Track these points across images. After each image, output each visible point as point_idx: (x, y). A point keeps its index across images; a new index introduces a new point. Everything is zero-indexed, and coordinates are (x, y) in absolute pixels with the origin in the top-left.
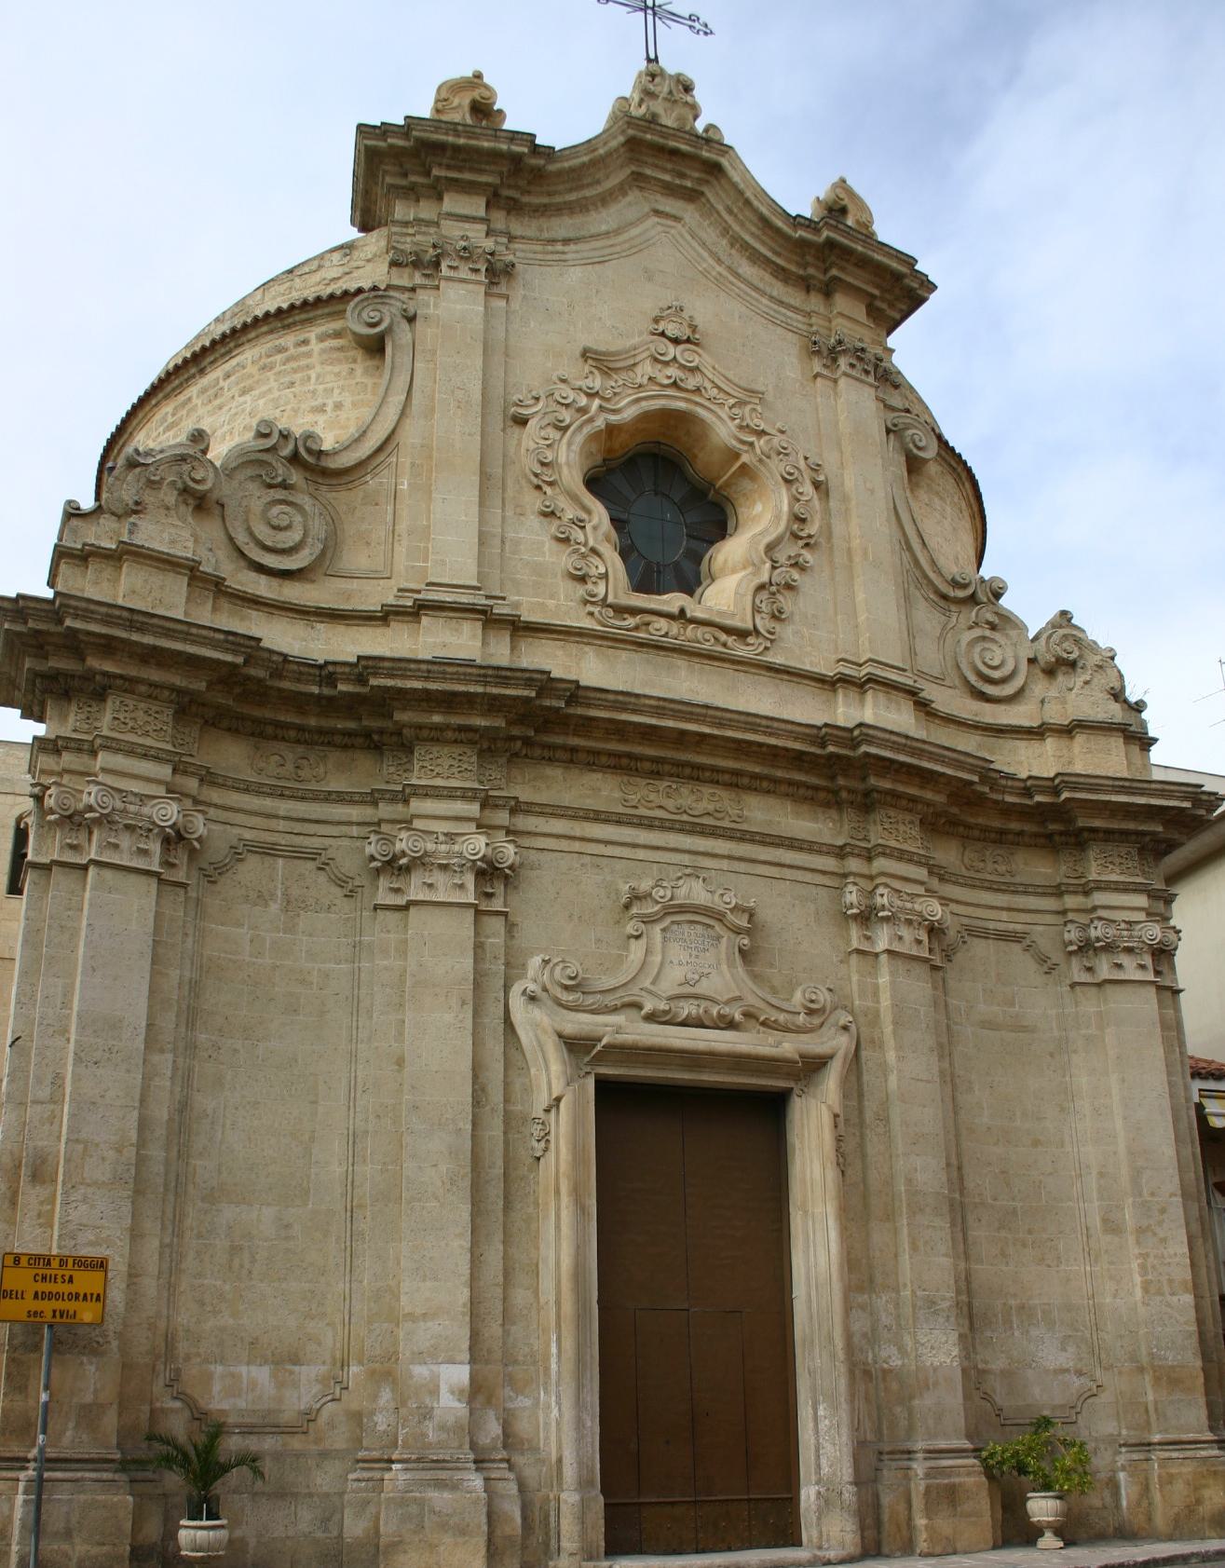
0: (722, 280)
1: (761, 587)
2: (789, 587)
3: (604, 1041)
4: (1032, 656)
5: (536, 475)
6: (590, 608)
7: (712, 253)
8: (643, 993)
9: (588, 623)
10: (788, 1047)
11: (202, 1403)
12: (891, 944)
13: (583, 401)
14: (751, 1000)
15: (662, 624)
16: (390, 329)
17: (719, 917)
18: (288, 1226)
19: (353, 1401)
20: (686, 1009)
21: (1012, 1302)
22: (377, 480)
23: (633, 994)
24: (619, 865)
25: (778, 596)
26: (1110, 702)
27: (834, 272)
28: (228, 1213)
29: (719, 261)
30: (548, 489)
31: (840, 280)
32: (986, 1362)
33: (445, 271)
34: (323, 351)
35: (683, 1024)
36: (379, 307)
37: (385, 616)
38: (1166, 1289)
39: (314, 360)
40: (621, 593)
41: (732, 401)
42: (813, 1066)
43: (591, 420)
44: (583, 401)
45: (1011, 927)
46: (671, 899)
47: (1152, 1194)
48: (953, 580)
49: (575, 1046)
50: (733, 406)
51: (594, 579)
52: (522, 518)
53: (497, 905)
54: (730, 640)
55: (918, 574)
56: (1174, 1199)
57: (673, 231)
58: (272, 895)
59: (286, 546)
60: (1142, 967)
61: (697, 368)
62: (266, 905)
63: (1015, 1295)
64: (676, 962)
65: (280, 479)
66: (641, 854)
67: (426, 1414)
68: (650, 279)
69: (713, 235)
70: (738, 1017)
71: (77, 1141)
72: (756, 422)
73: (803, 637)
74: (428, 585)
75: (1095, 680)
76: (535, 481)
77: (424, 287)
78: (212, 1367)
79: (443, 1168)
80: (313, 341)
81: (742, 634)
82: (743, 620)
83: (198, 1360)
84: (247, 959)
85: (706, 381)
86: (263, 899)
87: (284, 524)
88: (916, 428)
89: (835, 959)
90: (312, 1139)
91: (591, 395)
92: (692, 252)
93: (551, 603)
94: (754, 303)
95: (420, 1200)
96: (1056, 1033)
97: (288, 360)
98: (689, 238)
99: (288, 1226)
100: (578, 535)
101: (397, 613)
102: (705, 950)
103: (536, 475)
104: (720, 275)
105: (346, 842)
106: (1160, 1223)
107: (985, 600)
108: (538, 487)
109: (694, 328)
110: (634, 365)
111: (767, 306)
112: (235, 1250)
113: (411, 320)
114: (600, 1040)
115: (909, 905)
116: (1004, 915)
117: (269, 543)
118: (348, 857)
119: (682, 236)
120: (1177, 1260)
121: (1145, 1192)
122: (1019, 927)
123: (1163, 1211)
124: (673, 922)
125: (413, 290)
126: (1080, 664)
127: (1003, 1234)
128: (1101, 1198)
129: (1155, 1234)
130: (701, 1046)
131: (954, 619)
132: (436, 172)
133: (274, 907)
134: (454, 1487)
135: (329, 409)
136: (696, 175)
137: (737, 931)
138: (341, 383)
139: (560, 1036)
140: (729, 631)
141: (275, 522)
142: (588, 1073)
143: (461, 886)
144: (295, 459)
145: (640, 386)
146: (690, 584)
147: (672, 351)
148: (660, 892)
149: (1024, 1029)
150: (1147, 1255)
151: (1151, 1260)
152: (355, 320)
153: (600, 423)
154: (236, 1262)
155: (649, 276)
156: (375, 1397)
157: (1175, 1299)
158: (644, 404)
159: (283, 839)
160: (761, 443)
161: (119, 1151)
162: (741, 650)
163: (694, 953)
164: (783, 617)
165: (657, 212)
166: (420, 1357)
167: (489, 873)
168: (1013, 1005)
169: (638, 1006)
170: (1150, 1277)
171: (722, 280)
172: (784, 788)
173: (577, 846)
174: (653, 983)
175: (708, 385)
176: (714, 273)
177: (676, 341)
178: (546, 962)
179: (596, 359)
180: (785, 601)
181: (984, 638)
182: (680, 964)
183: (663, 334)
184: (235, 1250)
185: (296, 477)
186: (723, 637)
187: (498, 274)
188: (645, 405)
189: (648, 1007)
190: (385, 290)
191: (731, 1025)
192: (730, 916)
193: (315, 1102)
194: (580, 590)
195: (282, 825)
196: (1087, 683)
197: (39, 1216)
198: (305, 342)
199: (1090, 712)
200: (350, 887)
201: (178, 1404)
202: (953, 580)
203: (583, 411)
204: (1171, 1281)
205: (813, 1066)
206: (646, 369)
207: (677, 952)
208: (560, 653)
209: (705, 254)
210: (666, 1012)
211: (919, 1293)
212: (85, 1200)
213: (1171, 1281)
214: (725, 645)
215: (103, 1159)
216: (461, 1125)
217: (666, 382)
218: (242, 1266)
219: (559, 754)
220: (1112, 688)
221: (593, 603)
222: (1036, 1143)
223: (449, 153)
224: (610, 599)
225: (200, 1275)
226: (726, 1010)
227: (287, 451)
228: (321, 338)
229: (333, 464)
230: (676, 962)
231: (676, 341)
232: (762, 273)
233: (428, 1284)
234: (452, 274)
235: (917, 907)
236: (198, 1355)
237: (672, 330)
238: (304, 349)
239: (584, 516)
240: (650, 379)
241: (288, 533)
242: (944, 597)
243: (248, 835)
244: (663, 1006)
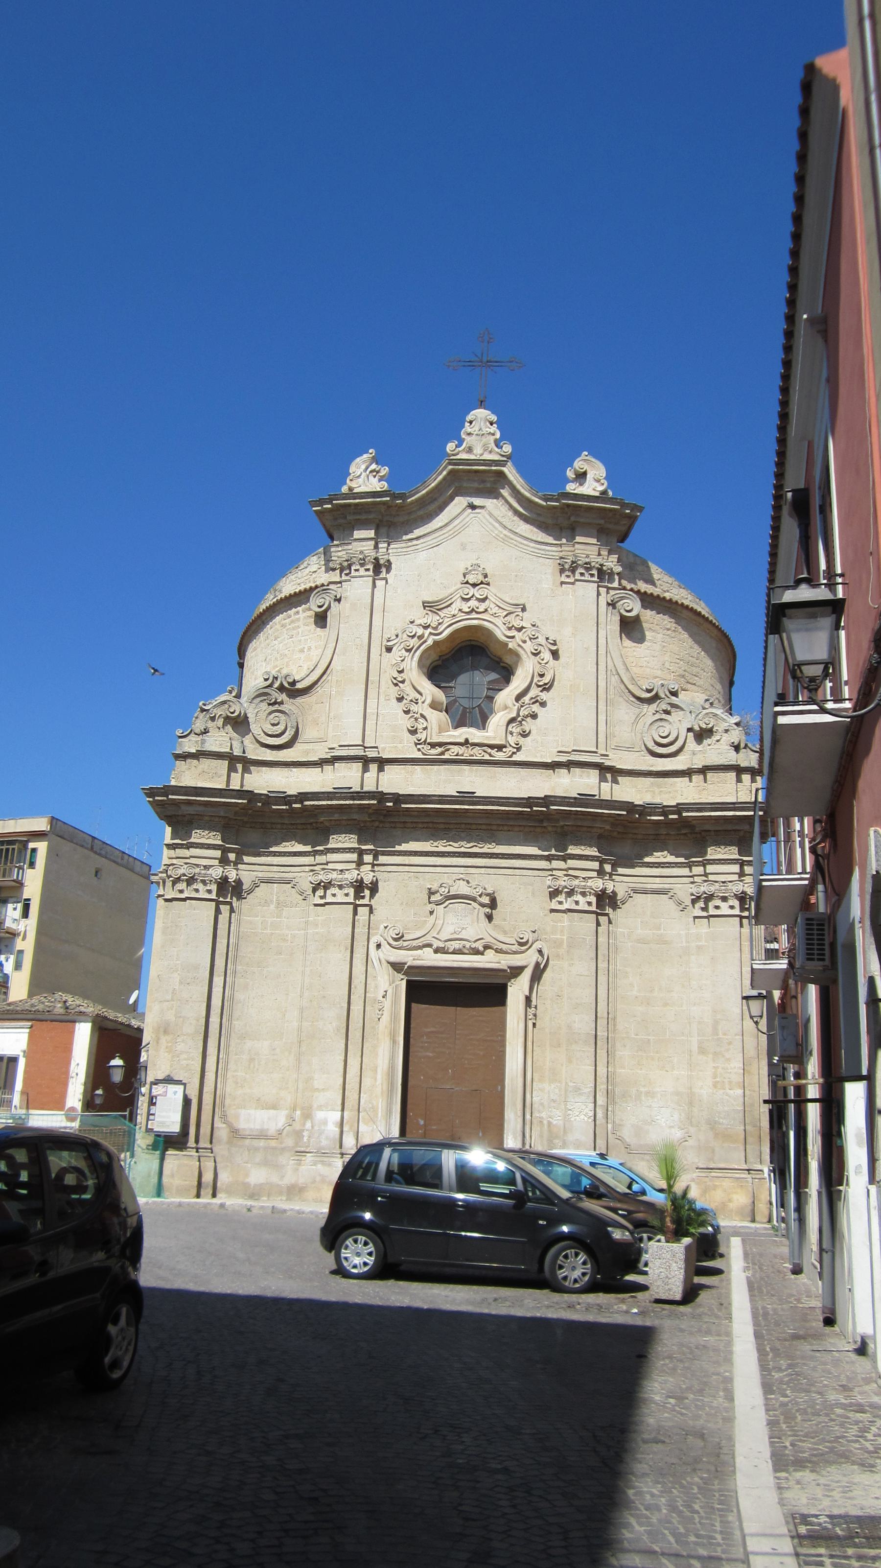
0: (506, 539)
1: (512, 720)
2: (534, 716)
3: (408, 964)
4: (689, 726)
5: (395, 679)
6: (419, 746)
7: (501, 523)
8: (433, 939)
9: (419, 755)
10: (502, 962)
11: (235, 1125)
12: (571, 905)
13: (420, 631)
14: (488, 939)
15: (455, 749)
16: (329, 607)
17: (474, 899)
18: (274, 1049)
19: (297, 1126)
20: (456, 945)
21: (642, 1089)
22: (323, 690)
23: (428, 939)
24: (427, 876)
25: (523, 722)
26: (731, 751)
27: (573, 519)
28: (249, 1044)
29: (505, 527)
30: (400, 684)
31: (578, 522)
32: (622, 1120)
33: (353, 573)
34: (305, 618)
35: (453, 953)
36: (324, 596)
37: (321, 763)
38: (727, 1086)
39: (300, 623)
40: (434, 735)
41: (505, 613)
42: (517, 971)
43: (425, 642)
44: (420, 631)
45: (661, 886)
46: (449, 892)
47: (725, 1034)
48: (647, 689)
49: (397, 967)
50: (506, 616)
51: (421, 731)
52: (389, 702)
53: (366, 901)
54: (493, 752)
55: (623, 687)
56: (737, 1037)
57: (479, 515)
58: (272, 901)
59: (277, 733)
60: (732, 907)
61: (486, 598)
62: (269, 906)
63: (644, 1086)
64: (450, 922)
65: (273, 700)
66: (438, 869)
67: (321, 1133)
68: (464, 549)
69: (504, 510)
70: (481, 949)
71: (180, 1017)
72: (517, 623)
73: (537, 742)
74: (340, 746)
75: (724, 738)
76: (395, 682)
77: (346, 581)
78: (240, 1110)
79: (334, 1024)
80: (301, 612)
81: (500, 748)
82: (501, 740)
83: (234, 1107)
84: (260, 931)
85: (492, 604)
86: (267, 903)
87: (276, 722)
88: (628, 598)
89: (542, 914)
90: (286, 1011)
91: (426, 627)
92: (490, 526)
93: (400, 746)
94: (526, 547)
95: (324, 1038)
96: (684, 944)
97: (292, 622)
98: (488, 517)
99: (274, 1049)
100: (414, 708)
101: (326, 762)
102: (466, 916)
103: (395, 679)
104: (505, 535)
105: (303, 874)
106: (728, 1050)
107: (663, 696)
108: (396, 685)
109: (486, 576)
110: (451, 604)
111: (532, 547)
112: (252, 1060)
113: (339, 600)
114: (406, 964)
115: (583, 884)
116: (658, 880)
117: (270, 733)
118: (305, 880)
119: (484, 517)
120: (736, 1070)
121: (720, 1033)
122: (666, 886)
123: (730, 1043)
124: (451, 903)
125: (340, 582)
126: (714, 729)
127: (640, 1053)
128: (699, 1035)
129: (723, 1056)
130: (455, 965)
131: (645, 710)
132: (348, 518)
133: (272, 907)
134: (330, 1165)
135: (305, 650)
136: (492, 479)
137: (483, 905)
138: (311, 636)
139: (388, 963)
140: (492, 747)
141: (273, 722)
142: (402, 979)
143: (347, 895)
144: (281, 688)
145: (454, 616)
146: (482, 721)
147: (472, 591)
148: (442, 890)
149: (665, 943)
150: (718, 1067)
151: (720, 1070)
152: (315, 603)
153: (430, 642)
154: (252, 1066)
155: (463, 547)
156: (304, 1124)
157: (732, 1092)
158: (454, 626)
159: (277, 875)
160: (519, 636)
161: (198, 1020)
162: (500, 756)
163: (460, 918)
164: (527, 732)
165: (473, 507)
166: (320, 1108)
167: (359, 887)
168: (659, 929)
169: (429, 945)
170: (718, 1080)
171: (506, 539)
172: (516, 829)
173: (407, 868)
174: (438, 934)
175: (492, 606)
176: (502, 536)
177: (474, 585)
178: (386, 927)
179: (428, 606)
180: (529, 725)
181: (661, 719)
182: (452, 924)
183: (467, 583)
184: (252, 1060)
185: (283, 697)
186: (489, 750)
187: (379, 568)
188: (455, 627)
189: (435, 946)
190: (328, 585)
191: (476, 952)
192: (478, 898)
193: (287, 994)
194: (413, 738)
195: (275, 869)
196: (718, 741)
197: (167, 1047)
198: (298, 613)
199: (716, 759)
200: (305, 895)
201: (224, 1125)
202: (647, 689)
203: (420, 637)
204: (730, 1082)
205: (517, 971)
206: (458, 604)
207: (451, 918)
208: (403, 771)
209: (497, 525)
210: (444, 948)
211: (571, 1084)
212: (183, 1041)
213: (730, 1082)
214: (490, 755)
215: (191, 1024)
216: (343, 1005)
217: (468, 610)
218: (254, 1067)
219: (398, 825)
220: (733, 743)
221: (419, 744)
222: (666, 1005)
223: (352, 507)
224: (428, 741)
225: (235, 1071)
226: (474, 945)
227: (276, 685)
228: (304, 611)
229: (299, 686)
230: (450, 922)
231: (474, 585)
232: (531, 527)
233: (325, 1076)
234: (357, 574)
235: (588, 884)
236: (234, 1105)
237: (472, 579)
238: (297, 617)
239: (418, 696)
240: (460, 610)
241: (279, 726)
242: (639, 699)
243: (260, 875)
244: (441, 945)
